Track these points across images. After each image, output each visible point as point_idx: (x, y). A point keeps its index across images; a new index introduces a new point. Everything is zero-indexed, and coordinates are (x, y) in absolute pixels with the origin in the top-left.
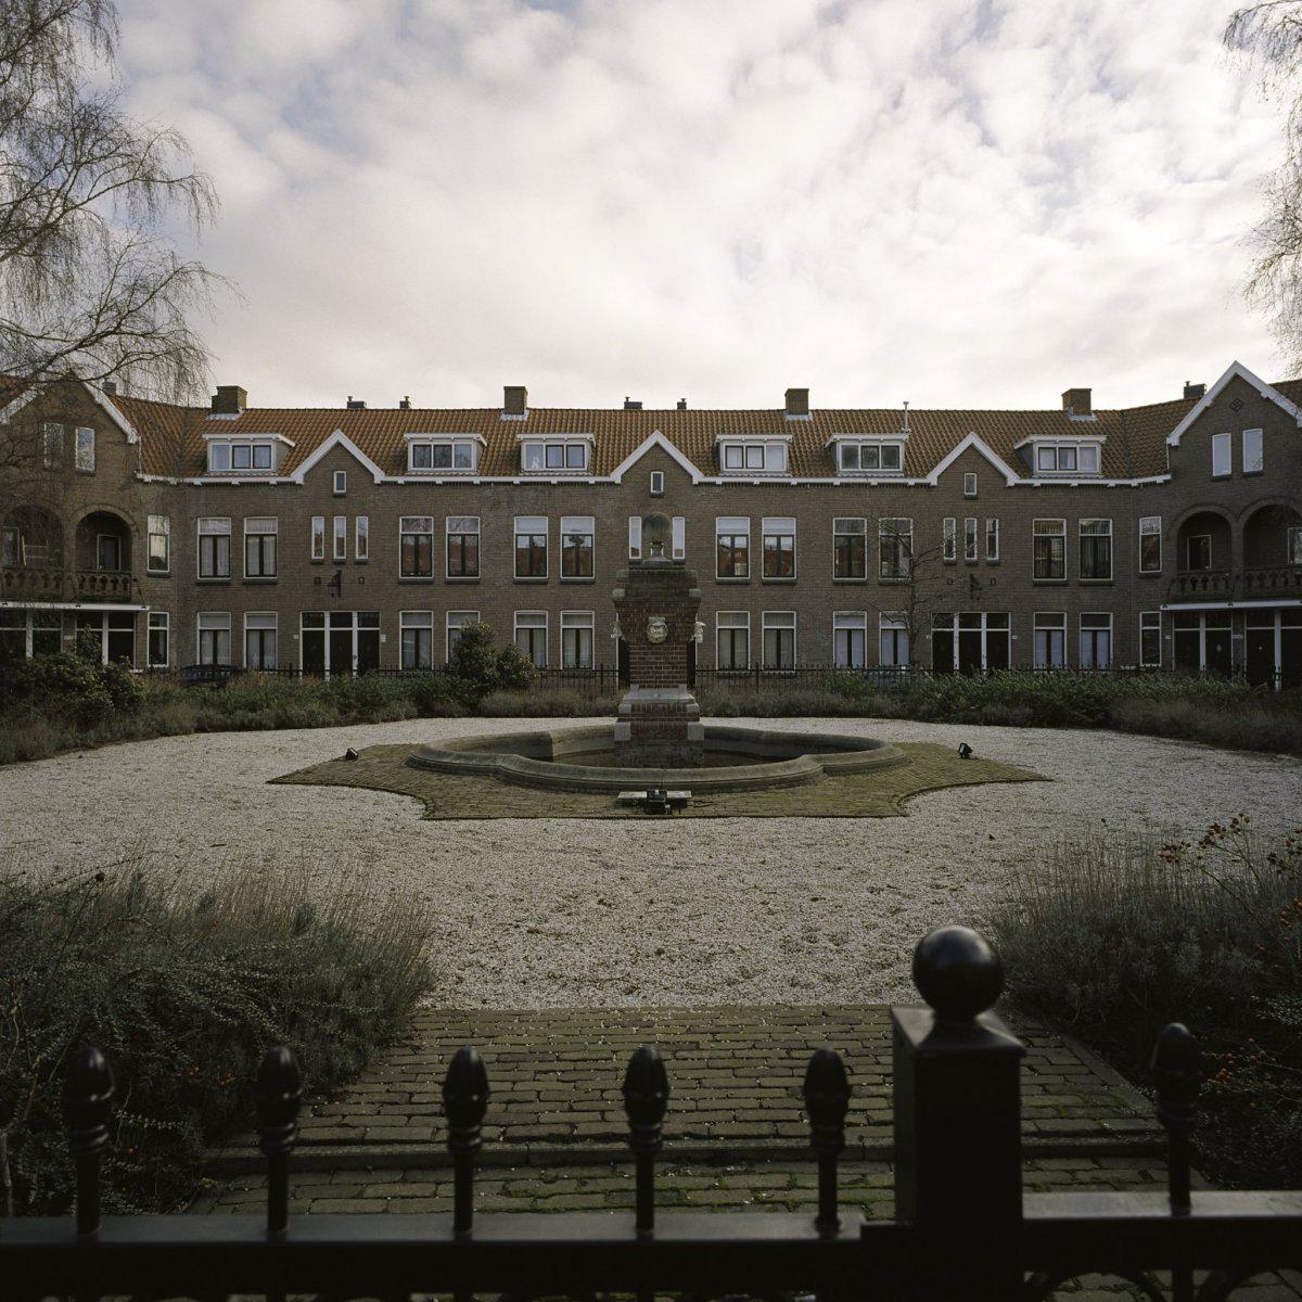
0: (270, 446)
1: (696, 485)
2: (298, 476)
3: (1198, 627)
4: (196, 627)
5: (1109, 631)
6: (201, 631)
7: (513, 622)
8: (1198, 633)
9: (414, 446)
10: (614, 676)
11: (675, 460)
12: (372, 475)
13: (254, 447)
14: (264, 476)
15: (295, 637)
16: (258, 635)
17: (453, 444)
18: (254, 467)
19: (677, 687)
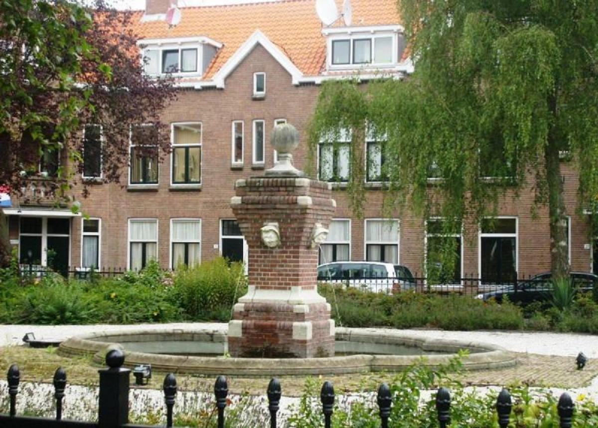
0: (196, 49)
1: (297, 86)
2: (218, 80)
3: (40, 232)
4: (127, 238)
5: (97, 237)
6: (131, 243)
7: (218, 234)
8: (40, 238)
9: (333, 42)
10: (466, 275)
11: (281, 65)
12: (290, 76)
13: (354, 41)
14: (191, 81)
15: (216, 246)
16: (140, 246)
17: (373, 37)
18: (354, 63)
19: (290, 289)
